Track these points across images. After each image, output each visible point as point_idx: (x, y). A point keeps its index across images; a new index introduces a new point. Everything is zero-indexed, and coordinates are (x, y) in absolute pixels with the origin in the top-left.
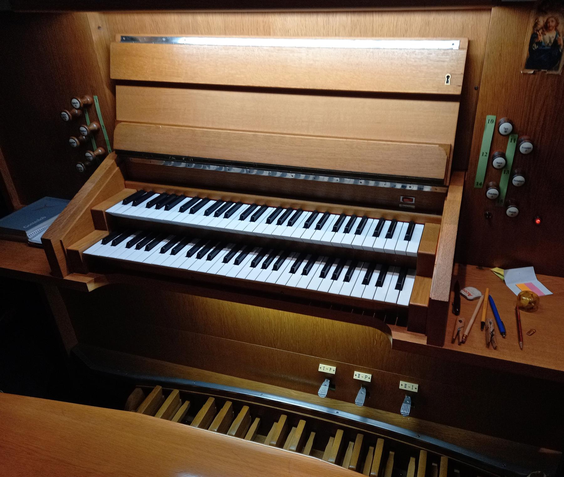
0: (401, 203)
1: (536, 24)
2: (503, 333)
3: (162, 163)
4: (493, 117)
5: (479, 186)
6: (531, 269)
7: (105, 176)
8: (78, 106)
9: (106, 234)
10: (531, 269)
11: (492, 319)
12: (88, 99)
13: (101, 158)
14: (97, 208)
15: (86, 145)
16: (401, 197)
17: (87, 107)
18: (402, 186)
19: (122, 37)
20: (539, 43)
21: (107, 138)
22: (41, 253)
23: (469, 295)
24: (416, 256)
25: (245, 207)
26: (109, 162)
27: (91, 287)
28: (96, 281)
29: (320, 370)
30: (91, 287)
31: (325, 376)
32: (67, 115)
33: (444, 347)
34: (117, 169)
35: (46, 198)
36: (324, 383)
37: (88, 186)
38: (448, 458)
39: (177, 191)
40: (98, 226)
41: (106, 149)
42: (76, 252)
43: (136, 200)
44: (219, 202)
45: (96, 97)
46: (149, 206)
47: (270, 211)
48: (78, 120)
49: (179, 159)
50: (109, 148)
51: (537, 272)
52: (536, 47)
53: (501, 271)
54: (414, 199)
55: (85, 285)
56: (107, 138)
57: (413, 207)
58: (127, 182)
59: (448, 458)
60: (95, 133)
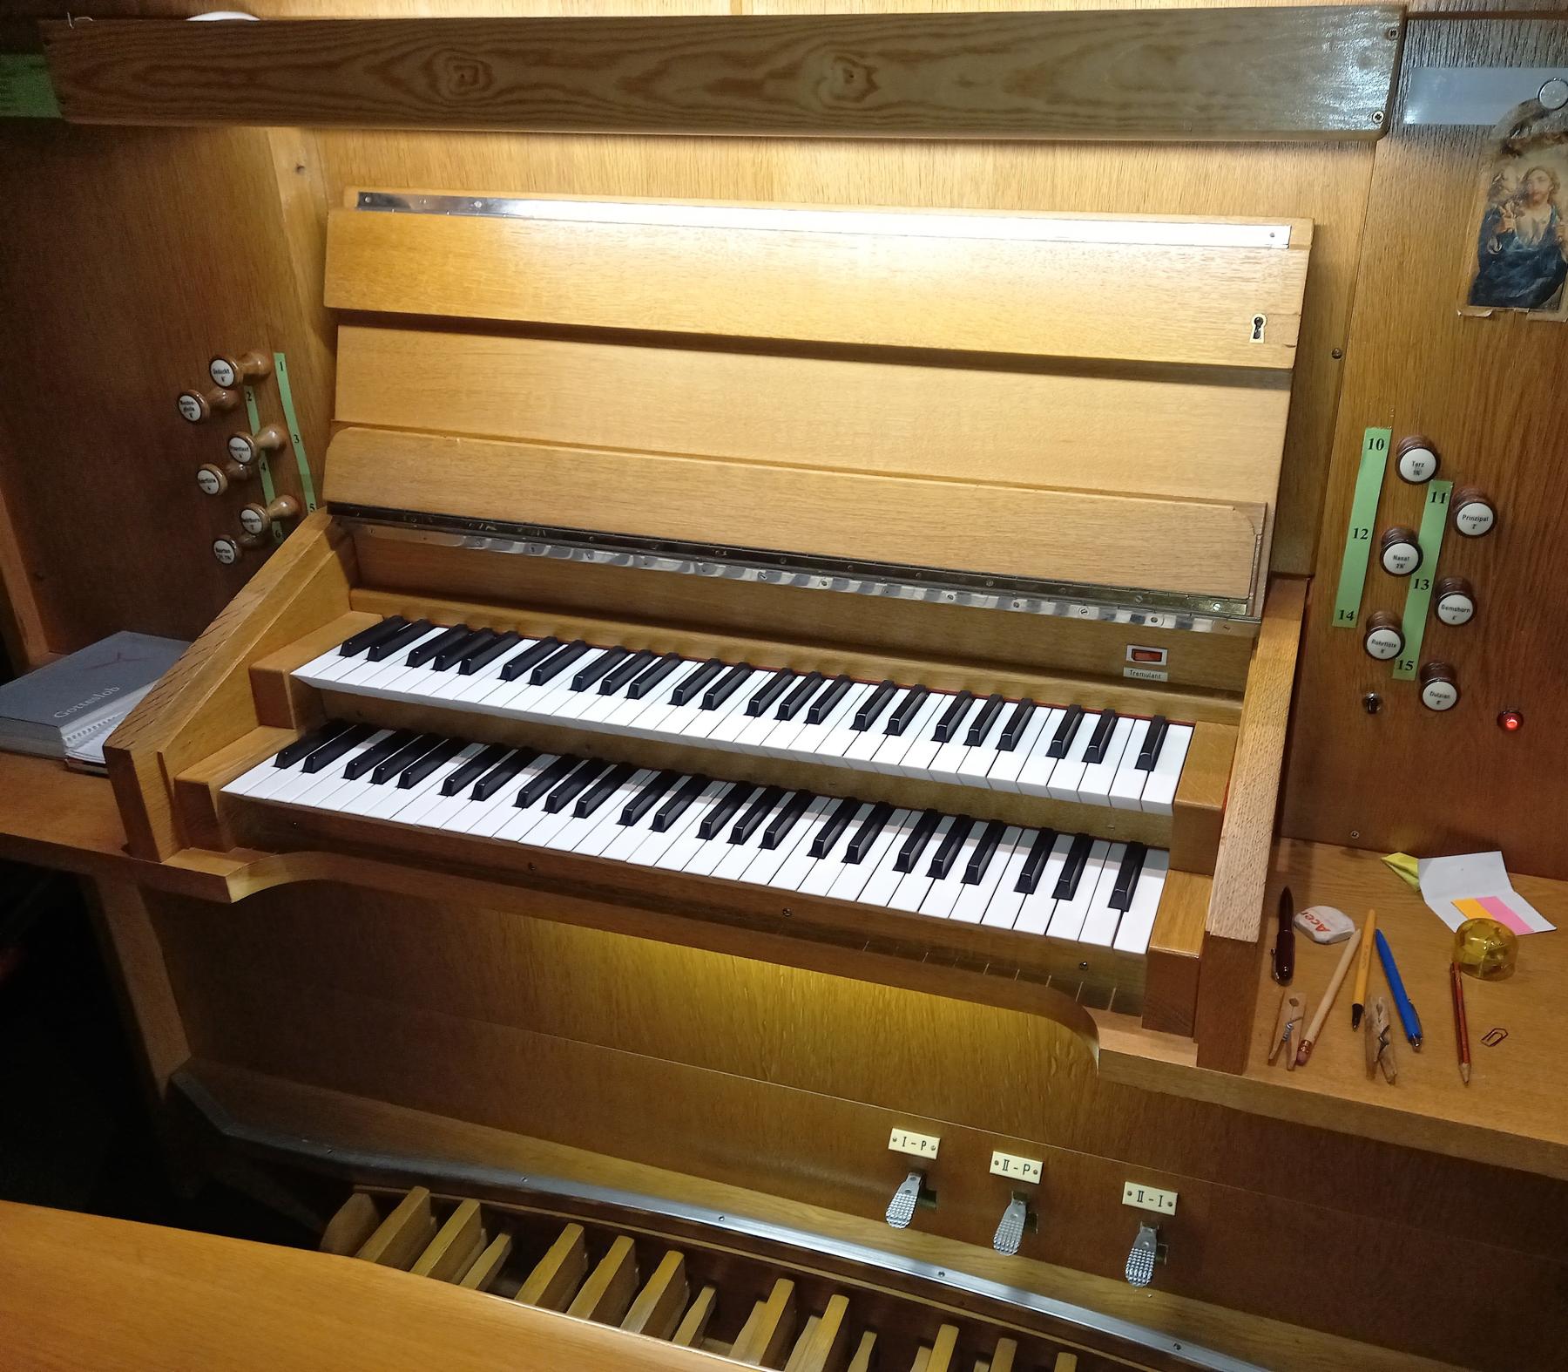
2: (1415, 1039)
3: (459, 541)
4: (1384, 434)
5: (1346, 623)
6: (1496, 857)
7: (296, 573)
8: (229, 379)
12: (259, 362)
13: (290, 523)
14: (268, 664)
15: (244, 488)
16: (1130, 648)
17: (255, 382)
18: (1133, 618)
19: (362, 195)
21: (304, 469)
22: (102, 792)
23: (1320, 928)
25: (759, 680)
26: (309, 535)
27: (238, 890)
28: (253, 873)
29: (890, 1148)
31: (905, 1164)
34: (331, 554)
35: (124, 634)
36: (903, 1187)
37: (247, 601)
38: (1479, 965)
40: (268, 715)
42: (202, 789)
43: (378, 643)
44: (785, 674)
46: (415, 660)
47: (758, 680)
48: (226, 417)
49: (509, 530)
51: (1513, 866)
54: (1165, 653)
55: (220, 883)
56: (304, 469)
58: (357, 593)
59: (1479, 965)
60: (274, 454)
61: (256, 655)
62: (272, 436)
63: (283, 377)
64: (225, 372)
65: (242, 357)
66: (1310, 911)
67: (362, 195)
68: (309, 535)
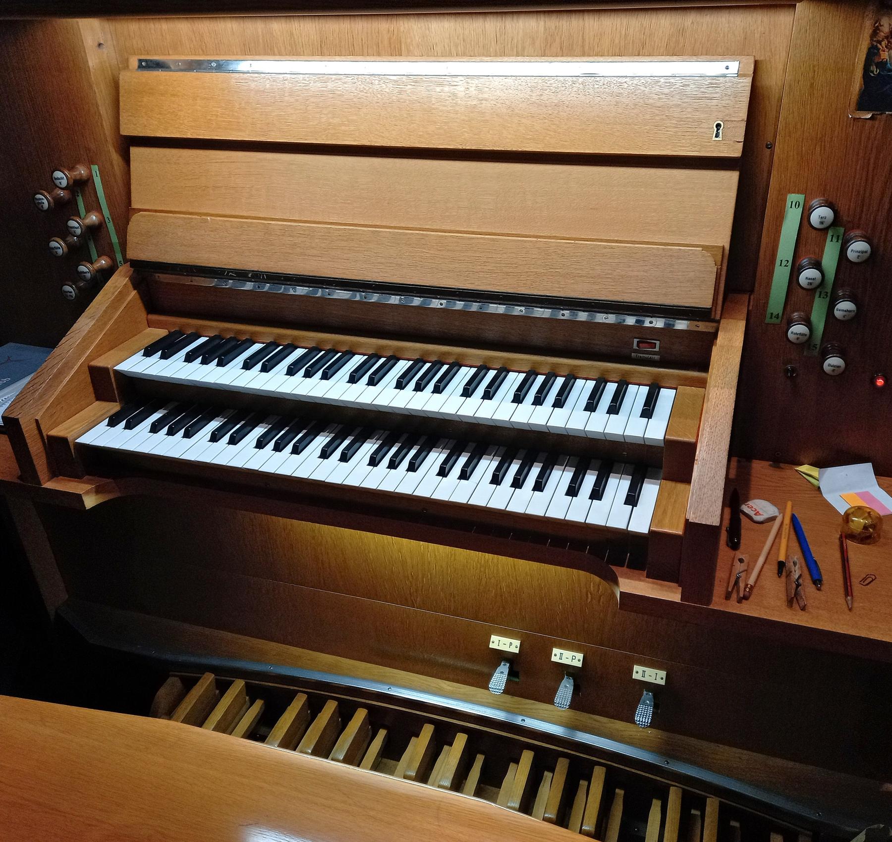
0: (635, 351)
1: (876, 31)
2: (817, 581)
3: (212, 283)
4: (800, 198)
8: (64, 183)
9: (115, 407)
10: (867, 468)
11: (797, 556)
12: (82, 171)
13: (106, 274)
14: (100, 362)
15: (79, 253)
16: (636, 341)
17: (80, 185)
18: (637, 321)
19: (140, 61)
20: (882, 65)
21: (114, 239)
23: (757, 513)
24: (662, 445)
26: (119, 281)
27: (90, 502)
28: (98, 491)
29: (490, 647)
30: (90, 502)
32: (45, 201)
33: (711, 607)
34: (134, 293)
36: (499, 669)
37: (84, 324)
39: (239, 332)
41: (113, 259)
42: (63, 441)
45: (95, 168)
49: (242, 275)
50: (119, 257)
52: (875, 70)
53: (815, 472)
55: (78, 498)
56: (114, 239)
57: (657, 357)
60: (95, 232)
61: (91, 357)
62: (93, 218)
63: (98, 181)
64: (61, 177)
65: (71, 168)
66: (750, 503)
67: (140, 61)
68: (119, 281)
